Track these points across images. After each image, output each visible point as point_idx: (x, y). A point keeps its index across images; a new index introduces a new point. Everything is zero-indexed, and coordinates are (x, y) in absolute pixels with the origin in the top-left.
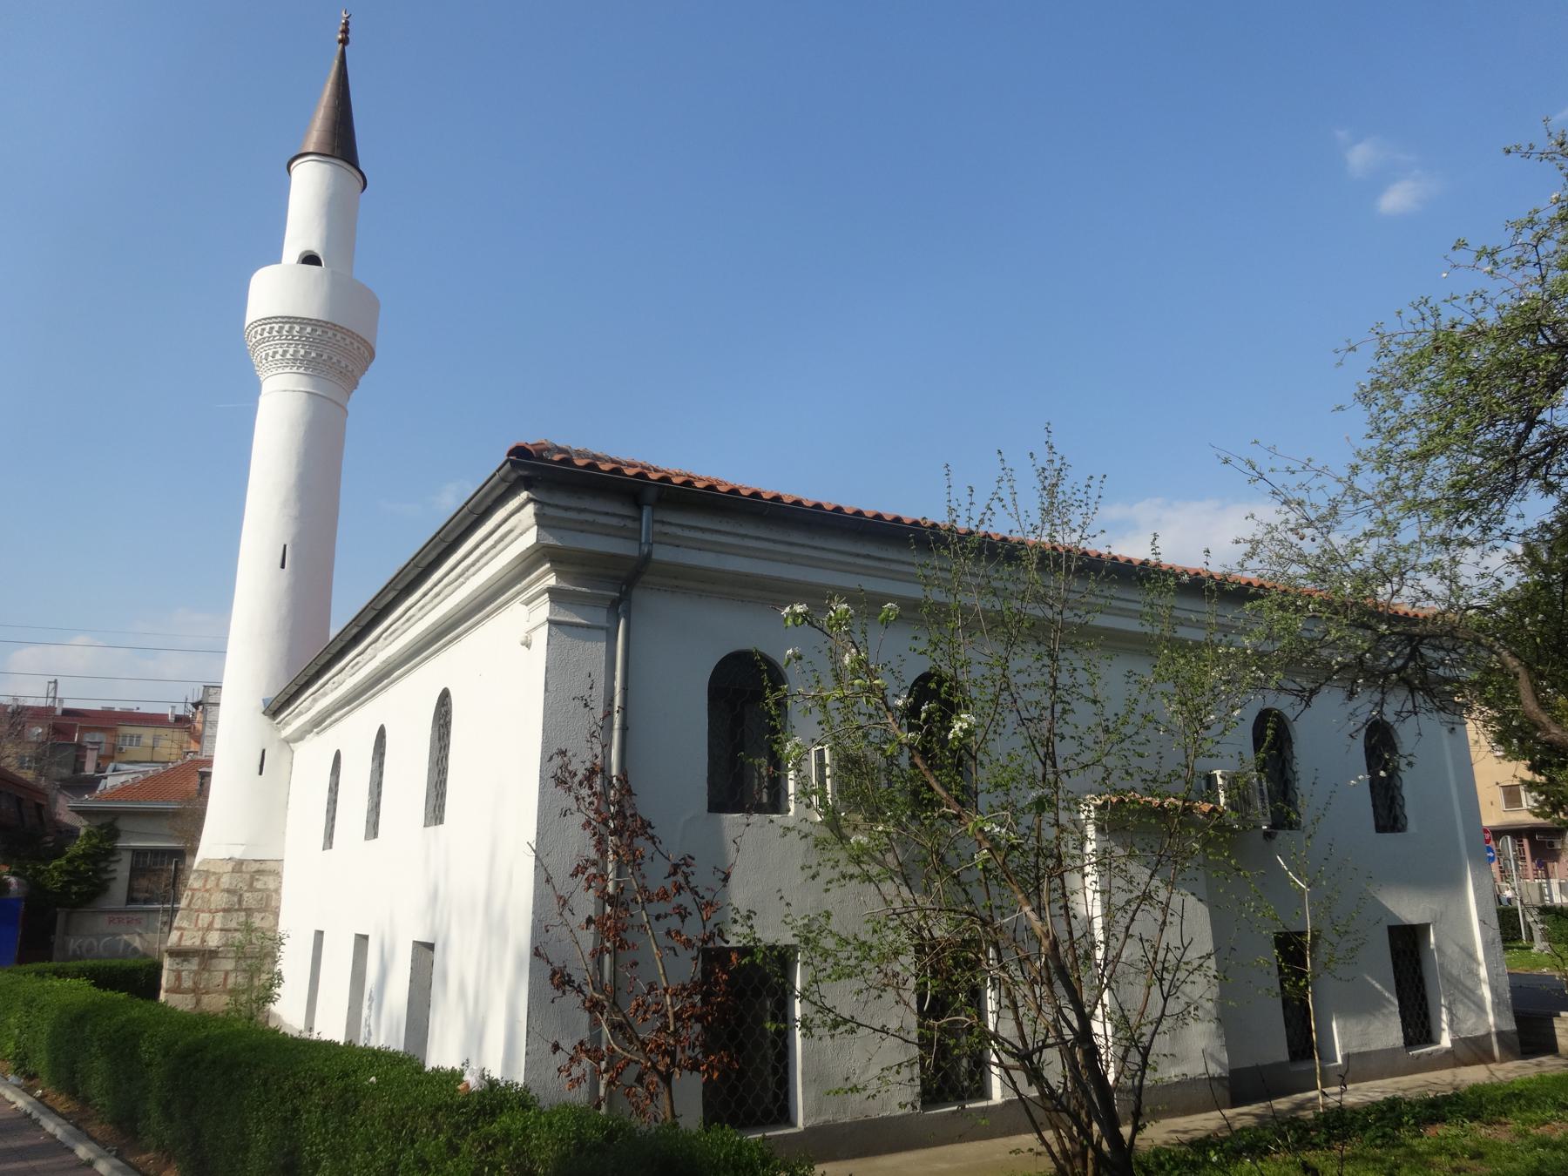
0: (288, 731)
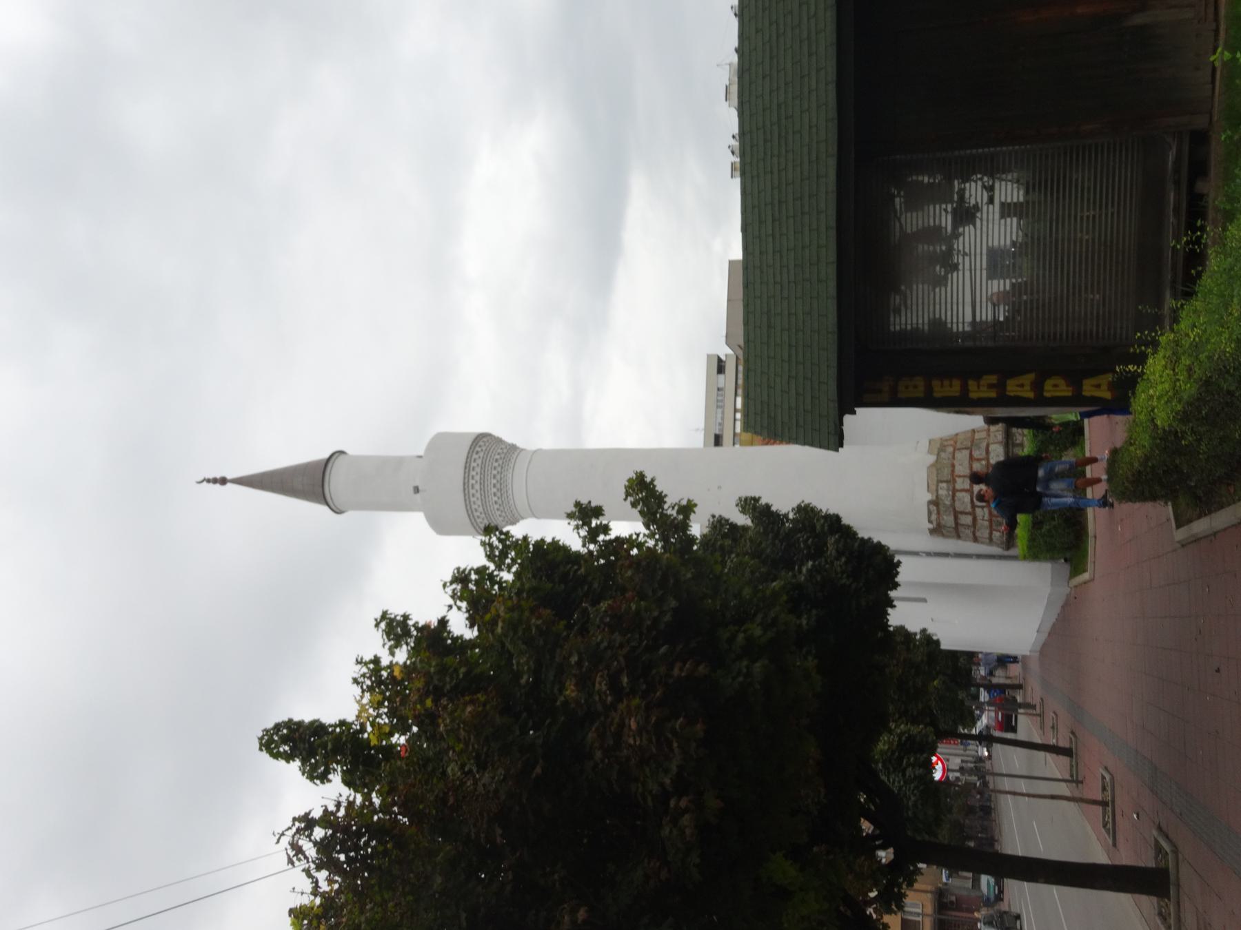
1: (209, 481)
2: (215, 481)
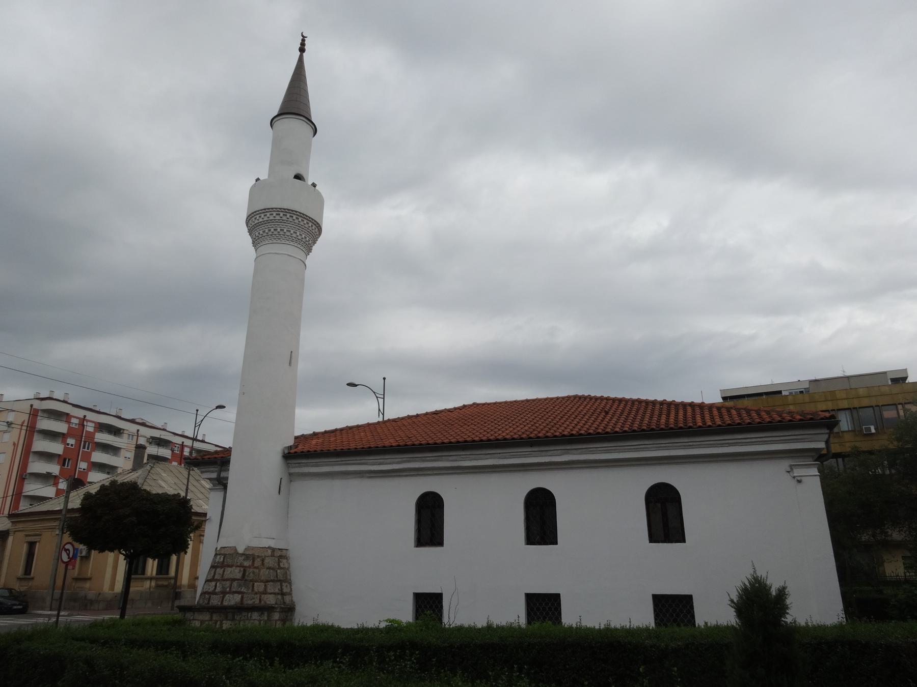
0: (293, 470)
1: (303, 40)
2: (303, 44)
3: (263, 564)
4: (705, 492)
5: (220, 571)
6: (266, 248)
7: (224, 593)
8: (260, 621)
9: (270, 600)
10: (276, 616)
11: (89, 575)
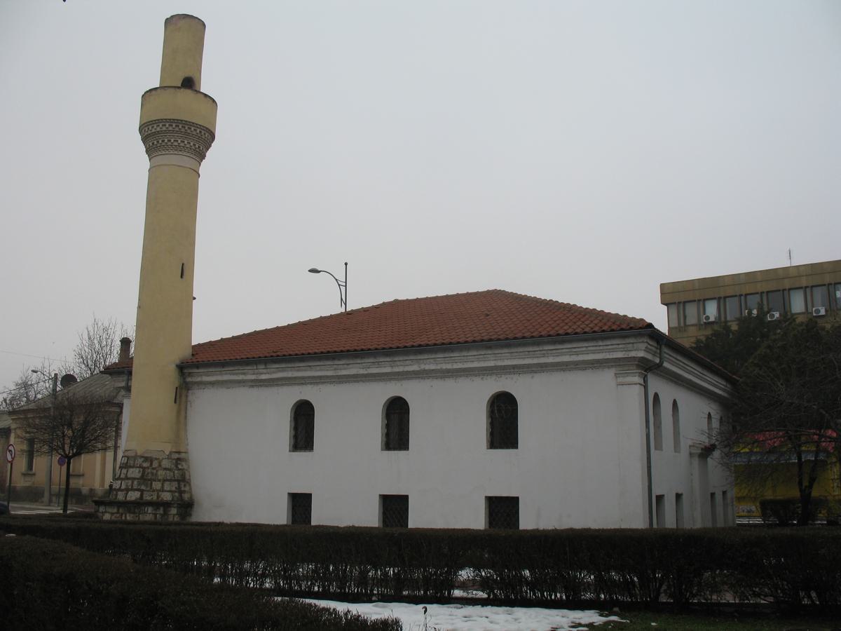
3: (160, 465)
4: (543, 400)
5: (124, 471)
6: (160, 160)
7: (127, 490)
8: (155, 515)
9: (167, 497)
10: (174, 511)
11: (81, 472)
